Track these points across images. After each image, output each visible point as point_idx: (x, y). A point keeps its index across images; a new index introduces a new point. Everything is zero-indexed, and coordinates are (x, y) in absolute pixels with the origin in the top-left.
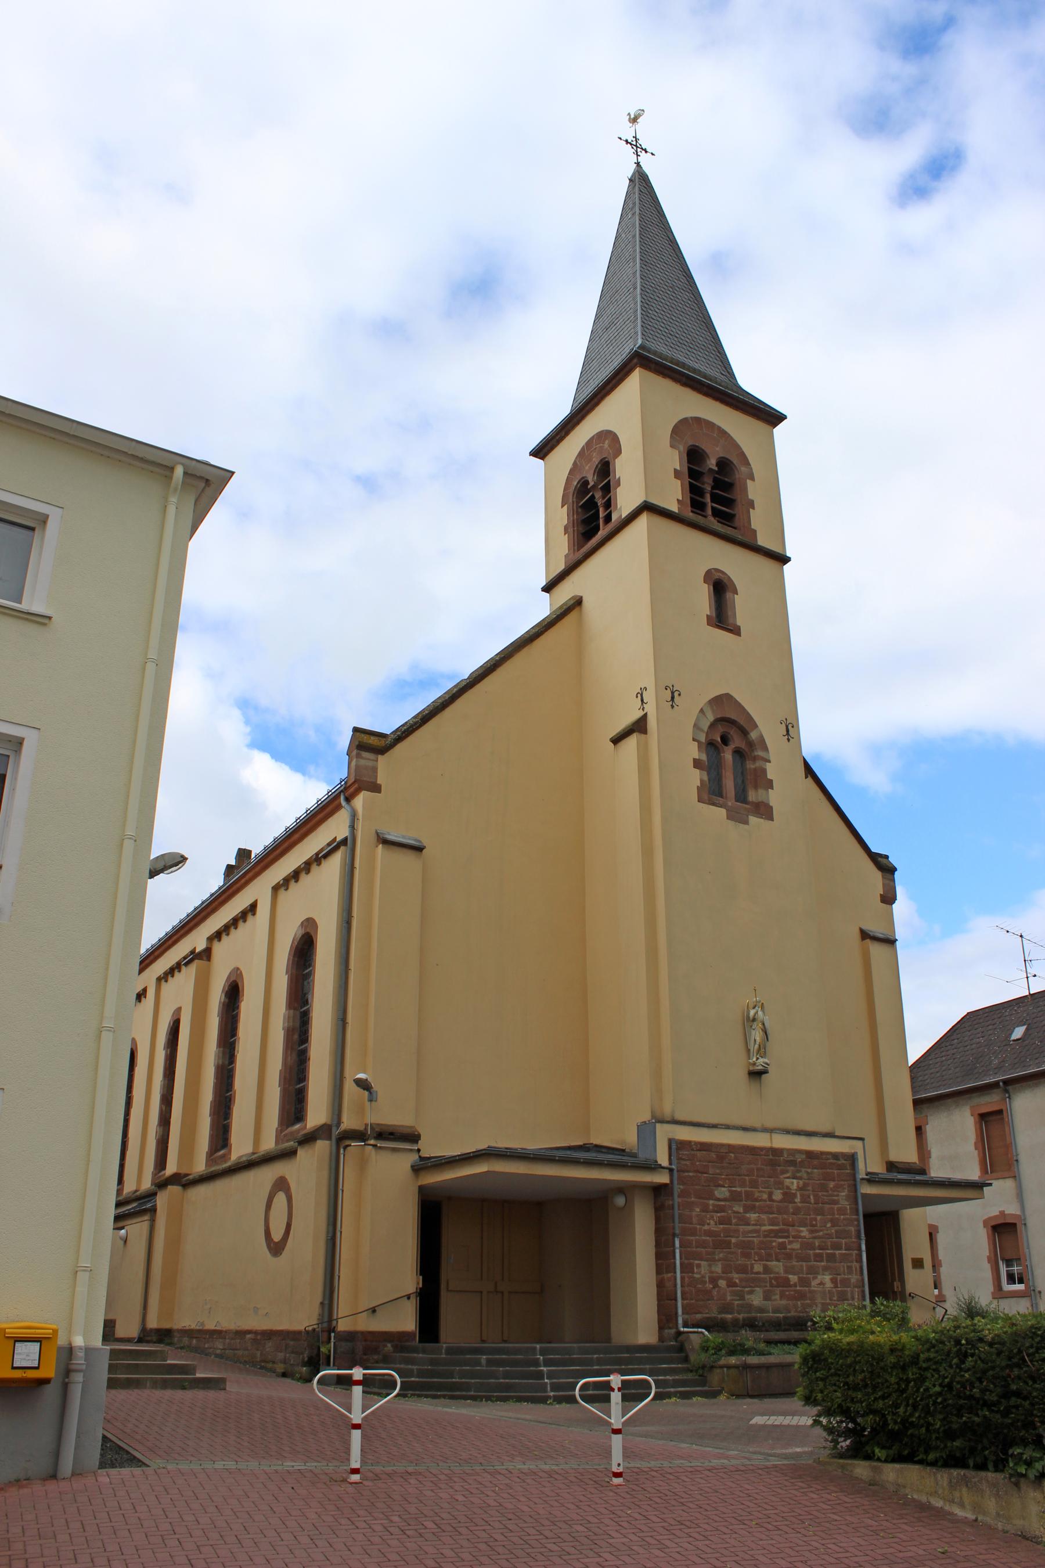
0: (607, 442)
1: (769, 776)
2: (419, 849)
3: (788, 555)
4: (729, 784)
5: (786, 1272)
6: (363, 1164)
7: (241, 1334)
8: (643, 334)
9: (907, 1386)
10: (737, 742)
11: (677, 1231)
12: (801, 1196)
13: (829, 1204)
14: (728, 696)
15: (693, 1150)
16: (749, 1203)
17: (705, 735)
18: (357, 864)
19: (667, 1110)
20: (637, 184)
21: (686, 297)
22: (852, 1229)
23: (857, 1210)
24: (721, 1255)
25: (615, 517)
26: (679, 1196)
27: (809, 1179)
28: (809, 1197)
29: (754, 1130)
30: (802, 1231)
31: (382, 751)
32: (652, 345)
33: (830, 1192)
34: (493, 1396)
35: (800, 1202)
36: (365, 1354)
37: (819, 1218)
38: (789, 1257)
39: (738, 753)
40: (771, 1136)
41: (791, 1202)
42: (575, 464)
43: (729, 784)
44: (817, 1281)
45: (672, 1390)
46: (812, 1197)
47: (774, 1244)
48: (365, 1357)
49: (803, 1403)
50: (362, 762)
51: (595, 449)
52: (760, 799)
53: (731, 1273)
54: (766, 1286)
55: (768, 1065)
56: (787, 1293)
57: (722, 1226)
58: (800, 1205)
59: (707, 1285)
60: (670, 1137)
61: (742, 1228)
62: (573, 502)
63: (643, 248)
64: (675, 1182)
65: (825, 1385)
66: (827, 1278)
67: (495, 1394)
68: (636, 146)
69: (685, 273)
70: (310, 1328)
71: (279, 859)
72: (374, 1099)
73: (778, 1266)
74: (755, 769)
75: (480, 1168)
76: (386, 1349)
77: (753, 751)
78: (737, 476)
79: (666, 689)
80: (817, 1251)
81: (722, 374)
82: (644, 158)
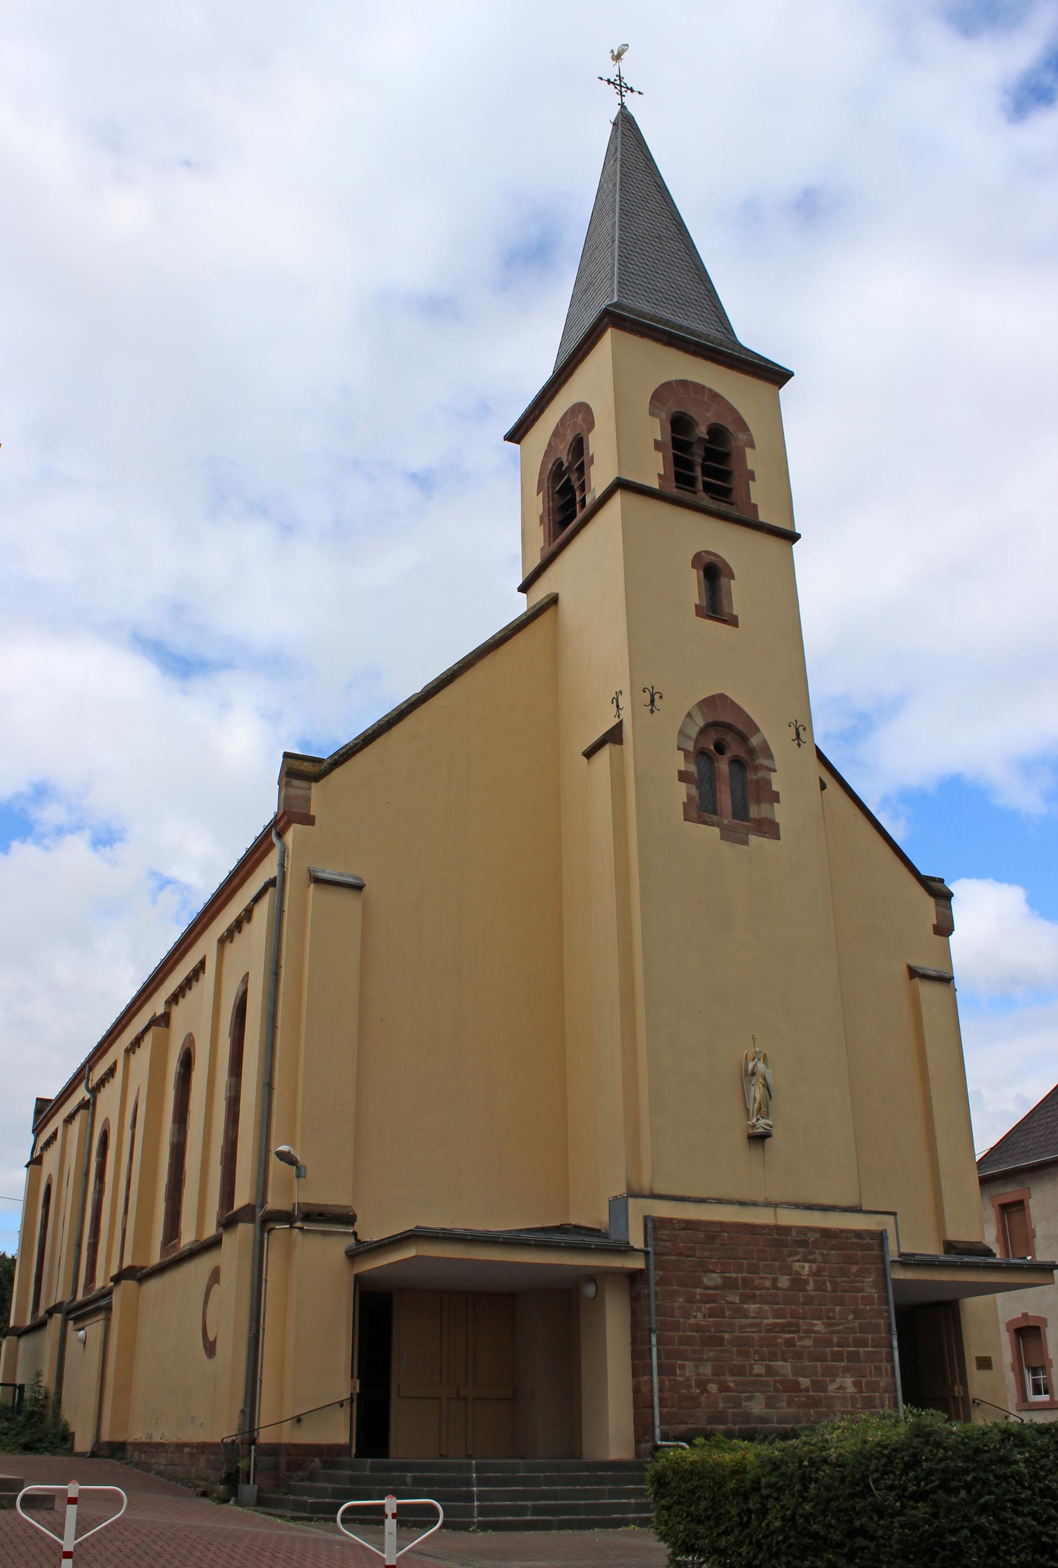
0: (580, 416)
1: (775, 788)
2: (358, 888)
3: (797, 531)
4: (725, 799)
5: (795, 1374)
6: (289, 1250)
7: (180, 1446)
8: (619, 291)
9: (749, 1518)
10: (734, 749)
11: (654, 1326)
12: (814, 1282)
13: (851, 1292)
14: (722, 697)
15: (675, 1229)
16: (747, 1291)
17: (693, 743)
18: (286, 908)
19: (646, 1183)
20: (620, 127)
21: (675, 247)
22: (882, 1321)
23: (887, 1299)
24: (711, 1354)
25: (588, 500)
26: (656, 1284)
27: (824, 1262)
28: (824, 1283)
29: (754, 1204)
30: (815, 1325)
31: (317, 777)
32: (631, 303)
33: (852, 1278)
34: (409, 1521)
35: (813, 1290)
36: (288, 1471)
37: (837, 1309)
38: (799, 1355)
39: (737, 762)
40: (775, 1211)
41: (800, 1290)
42: (550, 444)
43: (725, 799)
44: (835, 1385)
45: (631, 1516)
46: (828, 1284)
47: (779, 1340)
48: (288, 1474)
49: (658, 1537)
50: (293, 792)
51: (569, 425)
52: (763, 815)
53: (724, 1375)
54: (769, 1391)
55: (771, 1127)
56: (797, 1399)
57: (712, 1319)
58: (813, 1293)
59: (693, 1390)
60: (646, 1214)
61: (737, 1321)
62: (548, 487)
63: (624, 196)
64: (652, 1267)
65: (670, 1516)
66: (849, 1381)
67: (412, 1519)
68: (620, 85)
69: (676, 221)
70: (229, 1440)
71: (224, 908)
72: (303, 1175)
73: (785, 1368)
74: (757, 781)
75: (409, 1252)
76: (313, 1464)
77: (754, 759)
78: (733, 444)
79: (644, 691)
80: (836, 1349)
81: (718, 331)
82: (630, 100)
